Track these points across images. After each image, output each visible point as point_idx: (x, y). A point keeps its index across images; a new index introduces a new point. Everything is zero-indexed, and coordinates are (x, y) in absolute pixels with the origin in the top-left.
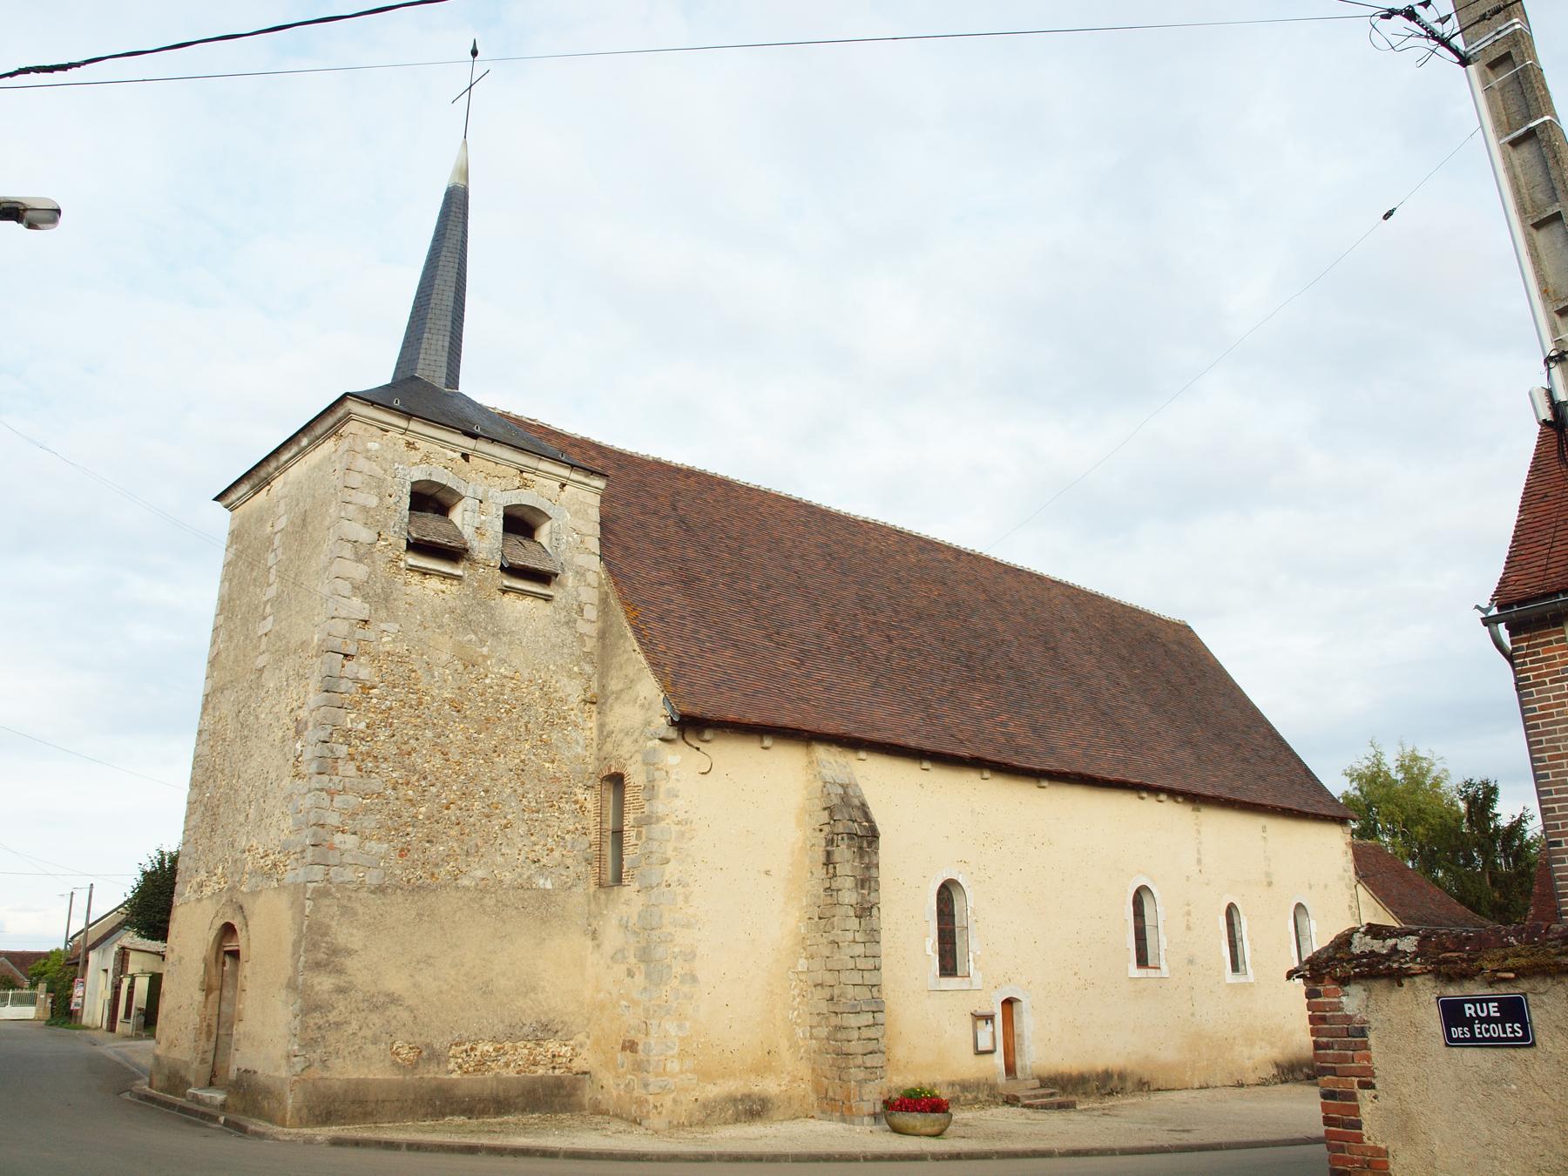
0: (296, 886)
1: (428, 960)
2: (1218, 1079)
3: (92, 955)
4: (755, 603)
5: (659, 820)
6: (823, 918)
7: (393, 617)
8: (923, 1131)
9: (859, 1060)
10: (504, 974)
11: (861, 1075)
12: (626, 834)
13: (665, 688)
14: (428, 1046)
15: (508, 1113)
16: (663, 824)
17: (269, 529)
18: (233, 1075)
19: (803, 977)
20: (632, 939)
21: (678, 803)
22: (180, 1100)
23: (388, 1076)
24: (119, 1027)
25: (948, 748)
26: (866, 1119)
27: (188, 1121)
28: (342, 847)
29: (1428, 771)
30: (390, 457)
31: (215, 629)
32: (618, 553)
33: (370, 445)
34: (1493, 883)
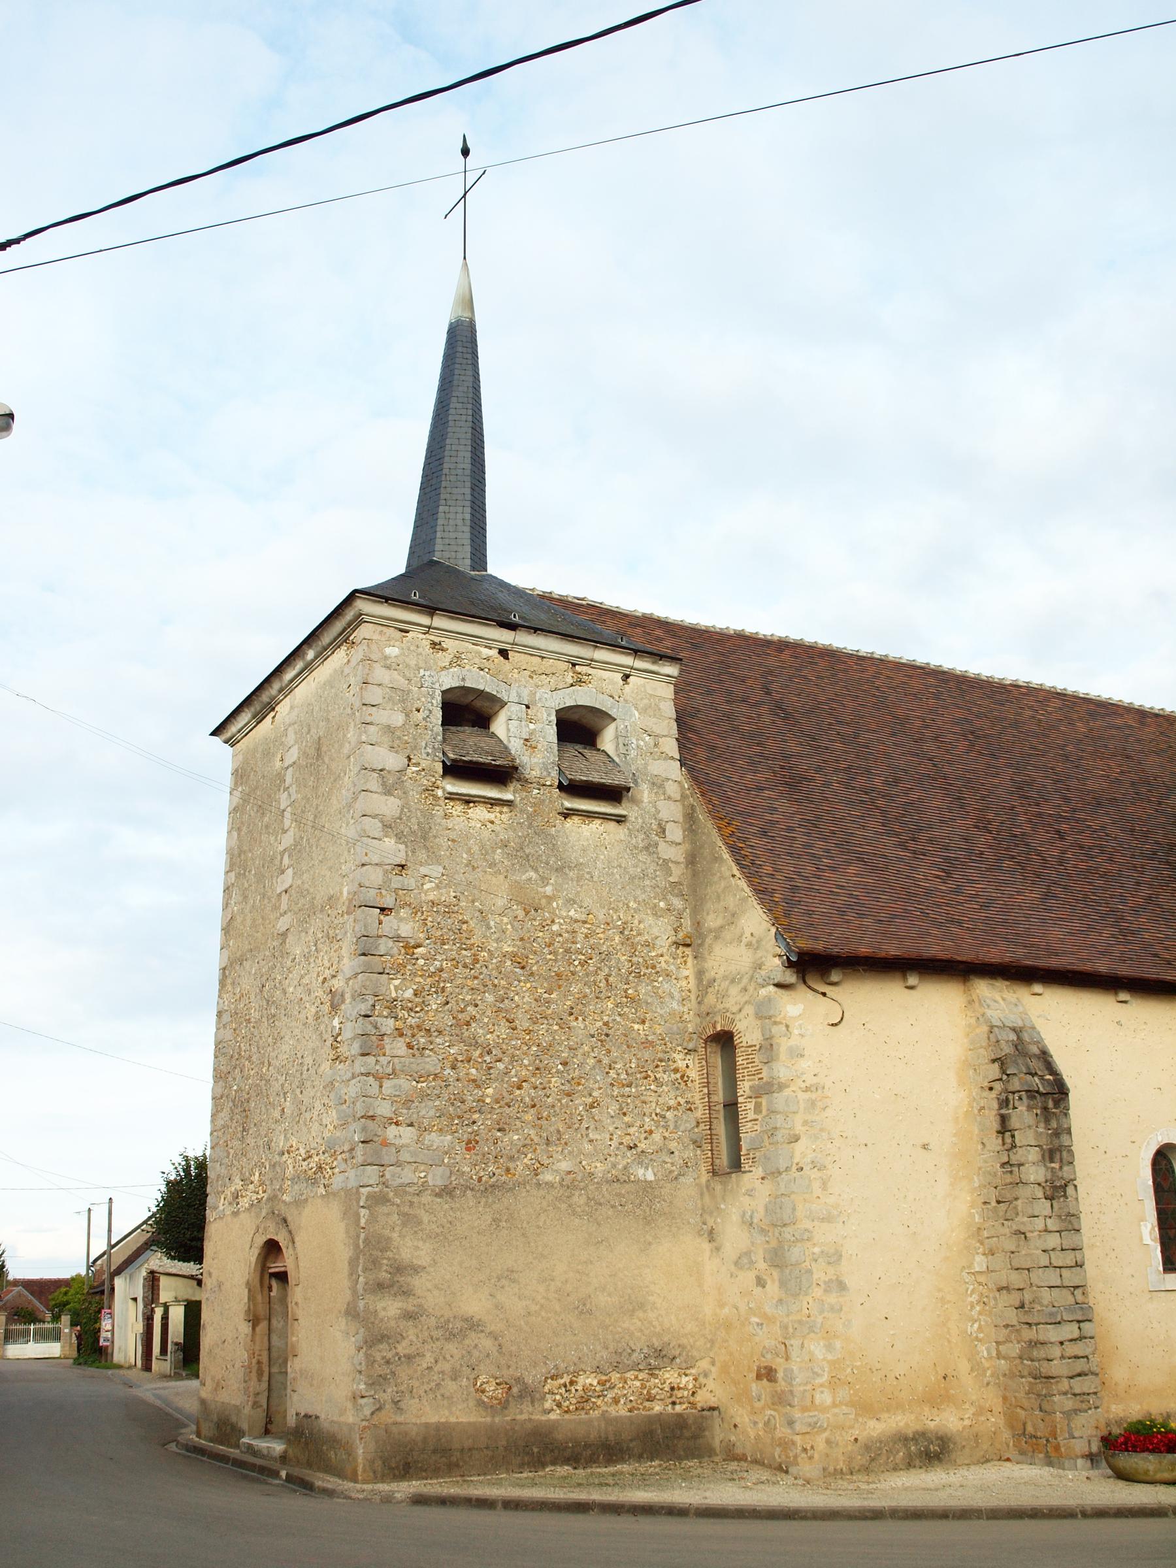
1: (510, 1275)
3: (118, 1282)
4: (880, 802)
5: (782, 1087)
6: (1002, 1200)
7: (434, 857)
8: (1159, 1476)
9: (1065, 1385)
11: (1069, 1403)
12: (741, 1107)
13: (776, 921)
14: (518, 1380)
15: (622, 1460)
16: (787, 1092)
18: (291, 1421)
19: (982, 1279)
20: (760, 1239)
21: (804, 1064)
22: (233, 1452)
24: (155, 1365)
26: (1080, 1462)
27: (245, 1477)
28: (398, 1142)
30: (413, 663)
31: (227, 890)
32: (702, 754)
33: (388, 651)
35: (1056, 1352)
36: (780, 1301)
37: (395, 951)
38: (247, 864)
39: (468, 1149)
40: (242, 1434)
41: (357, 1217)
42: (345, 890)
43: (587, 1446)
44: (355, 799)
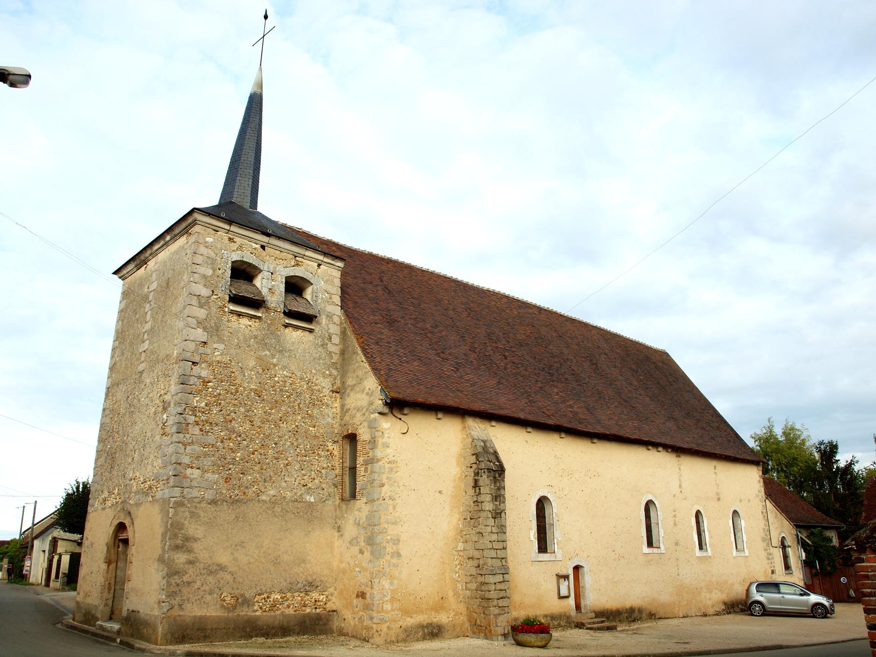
0: (164, 500)
1: (242, 544)
2: (693, 612)
3: (36, 542)
4: (429, 335)
5: (378, 461)
6: (473, 518)
7: (221, 340)
8: (536, 644)
9: (495, 602)
10: (286, 553)
11: (497, 611)
12: (358, 469)
13: (381, 383)
14: (242, 595)
15: (290, 635)
16: (380, 463)
17: (146, 290)
18: (125, 613)
19: (461, 553)
20: (362, 531)
21: (389, 451)
22: (92, 629)
23: (218, 614)
24: (52, 584)
25: (542, 420)
26: (500, 637)
27: (98, 642)
28: (192, 476)
29: (799, 436)
30: (219, 246)
31: (114, 349)
32: (351, 305)
33: (207, 239)
34: (836, 499)
35: (493, 587)
36: (370, 561)
37: (198, 383)
38: (125, 337)
39: (226, 482)
40: (98, 620)
41: (168, 512)
42: (175, 352)
43: (273, 628)
44: (184, 309)
